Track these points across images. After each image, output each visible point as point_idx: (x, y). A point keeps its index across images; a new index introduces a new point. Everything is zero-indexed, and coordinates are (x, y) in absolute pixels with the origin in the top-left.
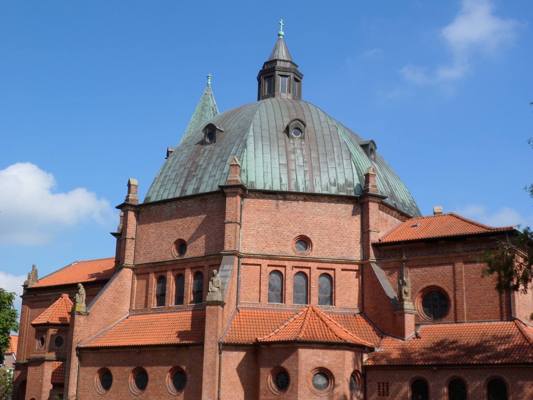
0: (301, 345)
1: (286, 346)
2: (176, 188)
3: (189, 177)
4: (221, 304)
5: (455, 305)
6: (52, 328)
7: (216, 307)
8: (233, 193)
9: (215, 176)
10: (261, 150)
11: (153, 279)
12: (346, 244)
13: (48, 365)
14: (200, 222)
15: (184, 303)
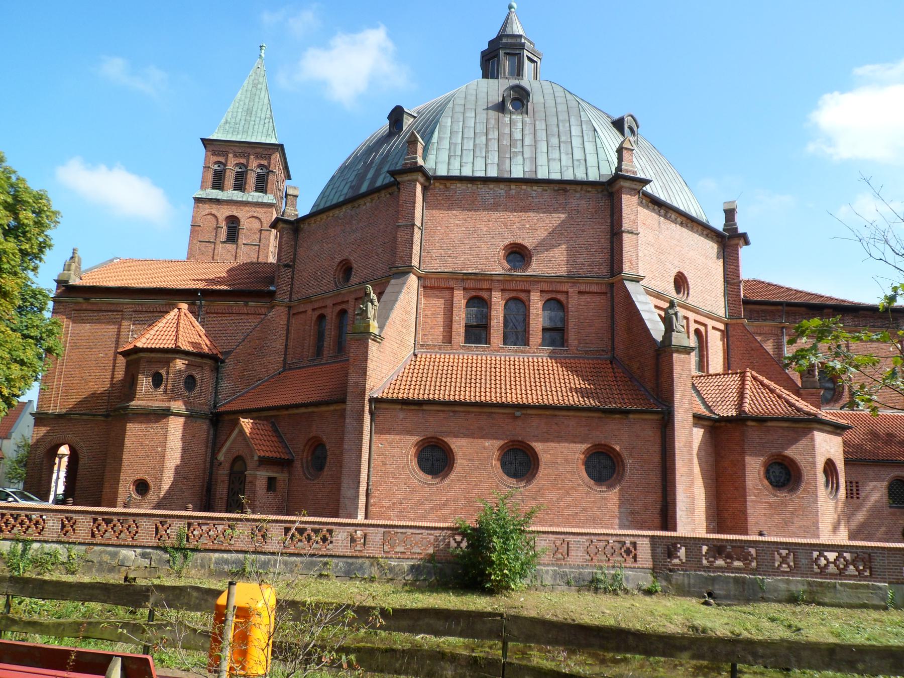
1: (794, 425)
6: (180, 359)
11: (460, 299)
13: (175, 422)
15: (531, 343)
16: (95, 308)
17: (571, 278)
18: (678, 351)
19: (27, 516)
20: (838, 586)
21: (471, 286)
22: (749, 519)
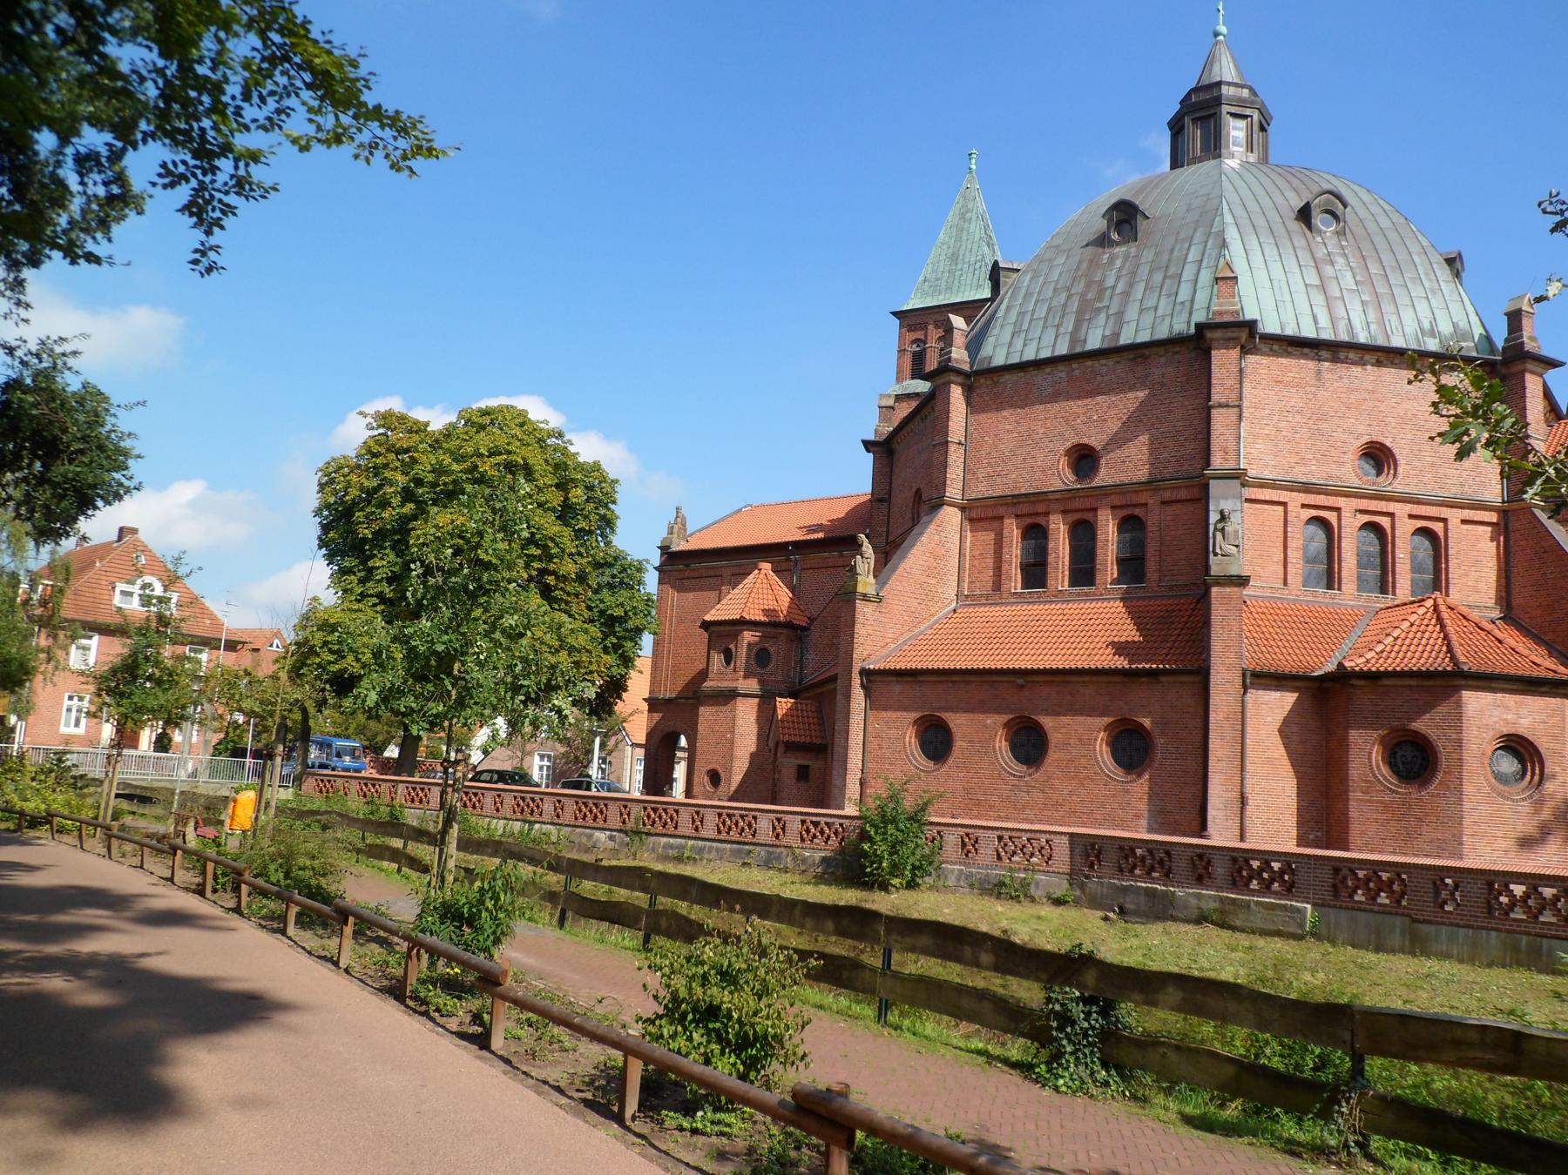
2: (1057, 337)
3: (1085, 314)
4: (1242, 581)
8: (1229, 339)
9: (1156, 308)
10: (1260, 253)
14: (1132, 406)
15: (1098, 582)
16: (696, 575)
17: (1151, 484)
18: (1218, 584)
22: (1352, 827)
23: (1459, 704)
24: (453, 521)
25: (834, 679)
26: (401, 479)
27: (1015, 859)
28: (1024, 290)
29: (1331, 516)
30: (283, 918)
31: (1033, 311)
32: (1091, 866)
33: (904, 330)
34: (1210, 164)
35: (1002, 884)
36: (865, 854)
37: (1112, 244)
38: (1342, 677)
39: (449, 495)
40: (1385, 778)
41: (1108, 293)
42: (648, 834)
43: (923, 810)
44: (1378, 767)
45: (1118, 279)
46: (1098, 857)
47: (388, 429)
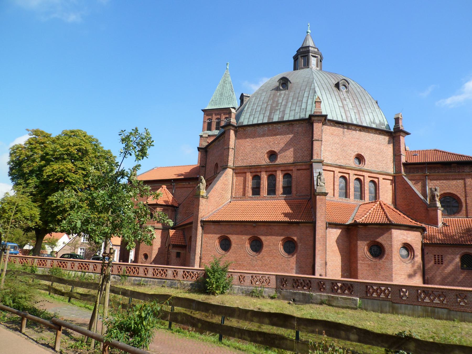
0: (394, 227)
2: (264, 117)
3: (273, 111)
4: (325, 194)
5: (466, 206)
7: (324, 197)
8: (319, 120)
9: (295, 110)
11: (249, 177)
12: (384, 162)
15: (276, 194)
17: (294, 164)
19: (192, 272)
20: (339, 298)
21: (253, 171)
23: (391, 234)
24: (59, 168)
25: (191, 223)
26: (41, 152)
27: (257, 283)
28: (253, 102)
29: (347, 176)
30: (21, 324)
31: (256, 109)
32: (283, 286)
33: (205, 115)
34: (306, 70)
35: (253, 292)
36: (207, 282)
37: (280, 90)
38: (355, 225)
39: (59, 159)
40: (369, 257)
41: (280, 104)
42: (128, 276)
43: (227, 267)
44: (366, 253)
45: (283, 100)
46: (285, 282)
47: (36, 135)
